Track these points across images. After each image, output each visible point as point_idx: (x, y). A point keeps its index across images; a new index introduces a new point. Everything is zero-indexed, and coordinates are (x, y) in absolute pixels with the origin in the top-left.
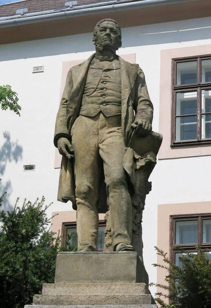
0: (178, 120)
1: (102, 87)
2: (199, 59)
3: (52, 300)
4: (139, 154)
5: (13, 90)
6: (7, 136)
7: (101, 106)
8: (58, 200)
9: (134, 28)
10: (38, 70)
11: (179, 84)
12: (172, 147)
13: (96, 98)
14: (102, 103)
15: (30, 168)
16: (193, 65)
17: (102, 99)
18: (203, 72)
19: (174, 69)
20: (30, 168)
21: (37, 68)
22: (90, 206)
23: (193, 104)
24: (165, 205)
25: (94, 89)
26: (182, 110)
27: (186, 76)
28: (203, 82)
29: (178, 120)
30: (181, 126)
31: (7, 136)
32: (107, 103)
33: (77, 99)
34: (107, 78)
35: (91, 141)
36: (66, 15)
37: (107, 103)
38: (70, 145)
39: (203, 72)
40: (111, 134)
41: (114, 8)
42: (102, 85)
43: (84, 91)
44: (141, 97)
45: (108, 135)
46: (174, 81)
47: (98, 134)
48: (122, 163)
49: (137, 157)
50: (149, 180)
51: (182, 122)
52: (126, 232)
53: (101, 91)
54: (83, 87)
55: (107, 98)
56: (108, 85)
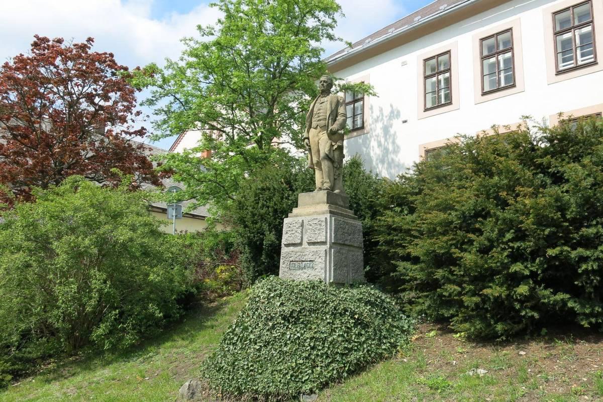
0: (486, 79)
2: (571, 8)
4: (334, 142)
5: (372, 84)
6: (391, 106)
9: (418, 40)
10: (404, 64)
11: (558, 29)
12: (482, 95)
15: (405, 122)
16: (493, 40)
17: (318, 119)
18: (576, 17)
19: (554, 20)
20: (405, 122)
21: (403, 63)
23: (569, 41)
26: (563, 47)
27: (562, 23)
28: (577, 23)
29: (560, 56)
30: (563, 59)
31: (391, 106)
32: (320, 120)
33: (309, 120)
36: (414, 27)
37: (320, 120)
39: (576, 17)
41: (440, 16)
42: (318, 112)
46: (554, 28)
49: (333, 144)
51: (505, 73)
52: (328, 181)
55: (321, 118)
56: (321, 111)
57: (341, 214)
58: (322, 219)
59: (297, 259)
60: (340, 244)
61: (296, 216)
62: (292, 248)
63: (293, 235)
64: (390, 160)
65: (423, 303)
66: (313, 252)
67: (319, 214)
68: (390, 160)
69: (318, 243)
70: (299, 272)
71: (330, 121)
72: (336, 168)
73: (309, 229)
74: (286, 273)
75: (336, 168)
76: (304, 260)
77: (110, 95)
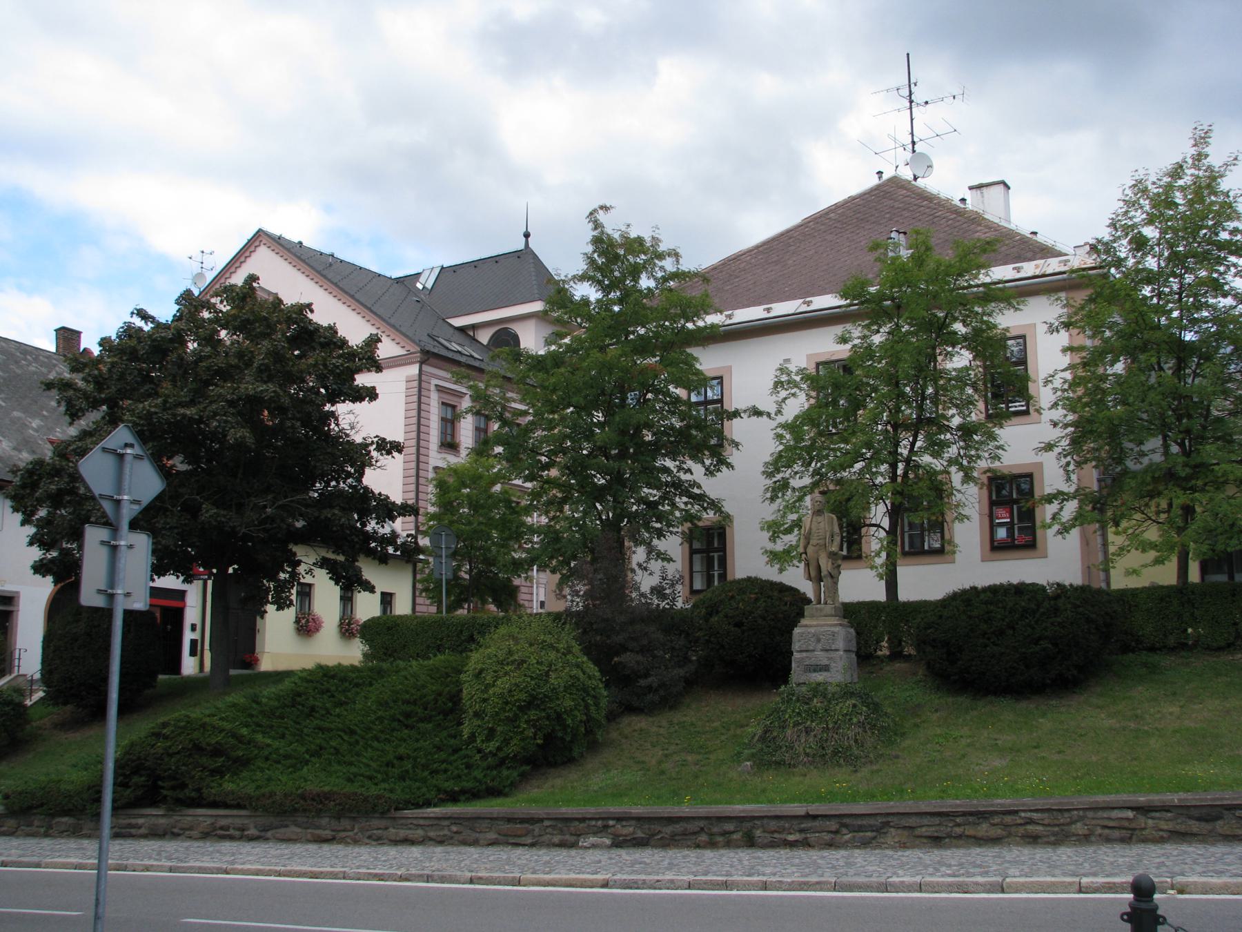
62: (804, 654)
70: (814, 675)
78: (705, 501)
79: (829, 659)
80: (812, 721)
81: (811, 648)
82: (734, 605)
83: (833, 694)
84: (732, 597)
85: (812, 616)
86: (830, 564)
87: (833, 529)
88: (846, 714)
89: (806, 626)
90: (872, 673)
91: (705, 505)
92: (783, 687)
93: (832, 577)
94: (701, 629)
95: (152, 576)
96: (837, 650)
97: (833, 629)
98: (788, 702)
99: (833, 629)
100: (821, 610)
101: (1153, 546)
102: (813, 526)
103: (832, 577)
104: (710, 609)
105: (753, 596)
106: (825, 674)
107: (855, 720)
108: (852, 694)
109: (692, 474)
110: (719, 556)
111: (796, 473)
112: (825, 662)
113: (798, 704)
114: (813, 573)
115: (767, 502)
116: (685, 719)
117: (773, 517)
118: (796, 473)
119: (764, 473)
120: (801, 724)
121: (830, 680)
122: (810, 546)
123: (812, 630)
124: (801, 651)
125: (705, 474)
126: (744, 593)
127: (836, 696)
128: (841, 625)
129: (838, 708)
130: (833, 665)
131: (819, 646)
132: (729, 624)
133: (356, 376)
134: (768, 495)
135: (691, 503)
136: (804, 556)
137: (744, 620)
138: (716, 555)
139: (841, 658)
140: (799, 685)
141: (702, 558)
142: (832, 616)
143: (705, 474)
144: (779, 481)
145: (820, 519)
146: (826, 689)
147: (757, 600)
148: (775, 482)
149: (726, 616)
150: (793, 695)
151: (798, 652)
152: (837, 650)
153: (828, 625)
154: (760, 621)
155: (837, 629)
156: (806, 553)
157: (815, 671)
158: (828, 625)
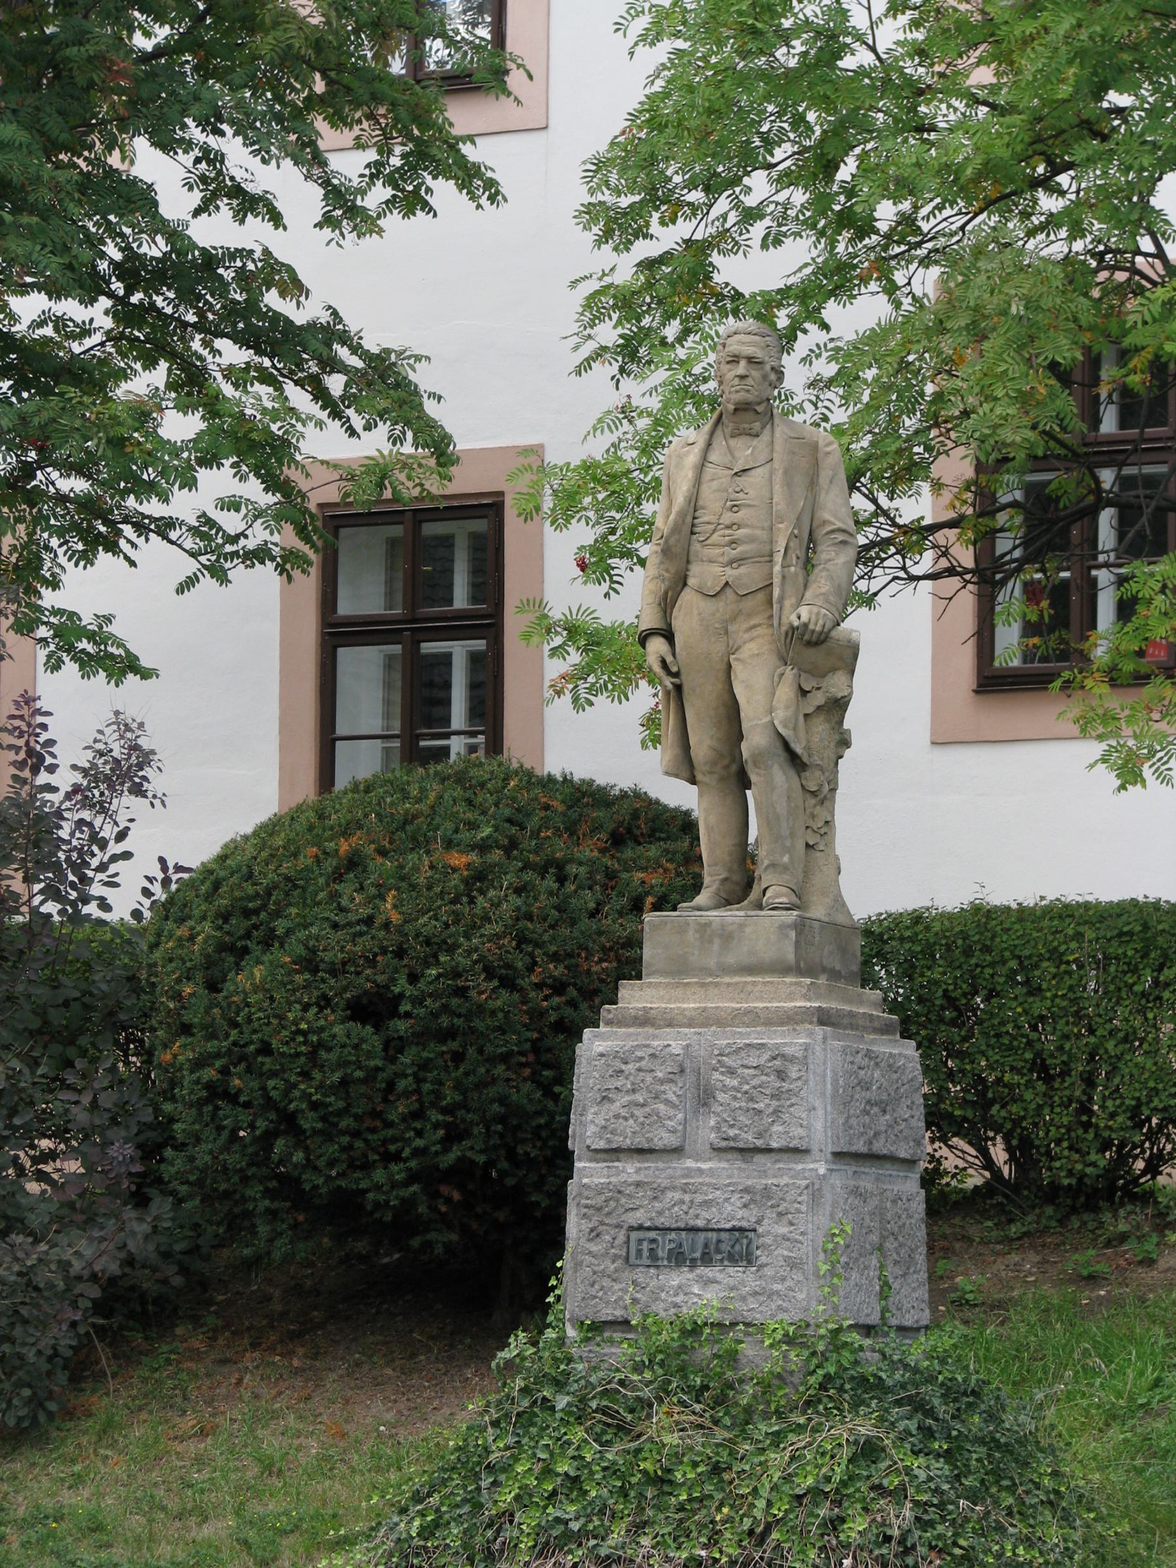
1: (727, 522)
3: (636, 1018)
7: (728, 569)
8: (667, 773)
13: (718, 551)
14: (731, 563)
22: (1082, 505)
24: (283, 748)
25: (712, 527)
34: (741, 495)
35: (851, 1490)
38: (669, 659)
40: (755, 633)
42: (728, 518)
43: (693, 525)
44: (825, 522)
45: (747, 636)
47: (727, 632)
48: (771, 711)
50: (846, 726)
53: (728, 532)
54: (689, 519)
56: (742, 514)
57: (748, 1012)
58: (788, 1050)
59: (662, 1221)
60: (857, 1157)
61: (644, 1020)
62: (630, 1169)
63: (639, 1112)
64: (225, 127)
65: (755, 1490)
66: (746, 1190)
67: (769, 1023)
68: (225, 127)
69: (651, 1151)
70: (675, 1278)
71: (777, 488)
72: (814, 794)
73: (725, 1089)
74: (606, 1282)
75: (814, 794)
76: (700, 1223)
77: (163, 365)
78: (332, 365)
79: (756, 1196)
80: (639, 1528)
81: (663, 1138)
82: (355, 902)
83: (766, 1387)
84: (354, 862)
85: (679, 969)
86: (786, 692)
87: (813, 507)
88: (816, 1493)
89: (644, 1020)
90: (1092, 1279)
91: (336, 384)
92: (517, 1344)
93: (795, 761)
94: (186, 1029)
95: (866, 963)
96: (798, 1152)
97: (777, 1038)
98: (525, 1419)
99: (777, 1038)
100: (727, 937)
101: (763, 427)
102: (711, 498)
103: (795, 761)
104: (238, 924)
105: (458, 859)
106: (734, 1274)
107: (857, 1526)
108: (870, 1386)
109: (276, 219)
110: (475, 659)
111: (750, 215)
112: (733, 1212)
113: (578, 1434)
114: (703, 744)
115: (605, 370)
116: (68, 1498)
117: (597, 448)
118: (750, 215)
119: (591, 212)
120: (578, 1538)
121: (755, 1311)
122: (687, 597)
123: (674, 1042)
124: (613, 1153)
125: (327, 221)
126: (419, 842)
127: (782, 1395)
128: (824, 1018)
129: (777, 1458)
130: (773, 1228)
131: (706, 1131)
132: (324, 1002)
133: (1111, 92)
134: (608, 333)
135: (266, 378)
136: (657, 646)
137: (402, 985)
138: (459, 651)
139: (816, 1196)
140: (596, 1328)
141: (389, 661)
142: (784, 970)
143: (327, 221)
144: (664, 259)
145: (745, 451)
146: (732, 1358)
147: (479, 878)
148: (649, 265)
149: (310, 963)
150: (560, 1384)
151: (597, 1154)
152: (798, 1152)
153: (754, 1018)
154: (482, 989)
155: (793, 1041)
156: (668, 636)
157: (678, 1258)
158: (754, 1018)
